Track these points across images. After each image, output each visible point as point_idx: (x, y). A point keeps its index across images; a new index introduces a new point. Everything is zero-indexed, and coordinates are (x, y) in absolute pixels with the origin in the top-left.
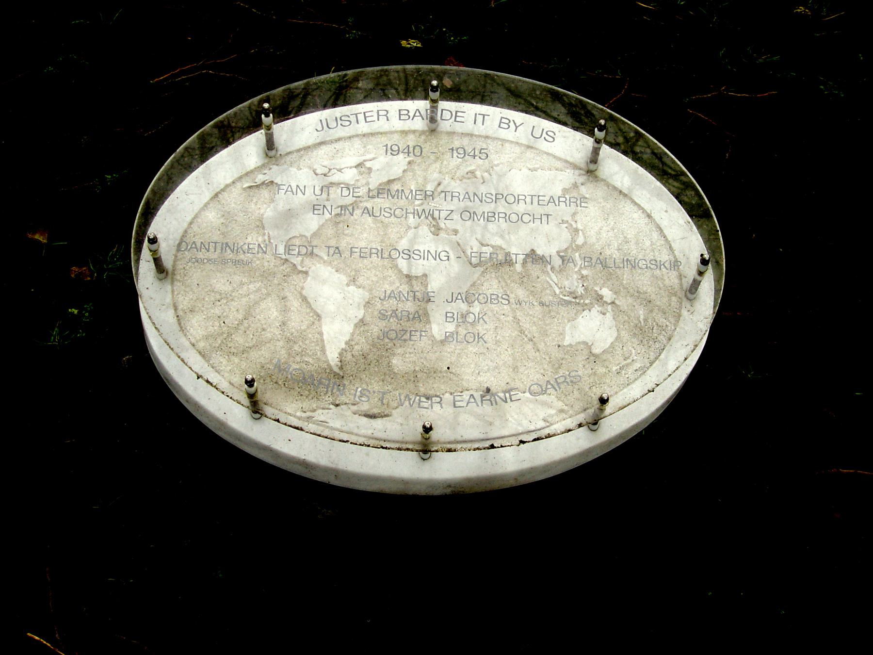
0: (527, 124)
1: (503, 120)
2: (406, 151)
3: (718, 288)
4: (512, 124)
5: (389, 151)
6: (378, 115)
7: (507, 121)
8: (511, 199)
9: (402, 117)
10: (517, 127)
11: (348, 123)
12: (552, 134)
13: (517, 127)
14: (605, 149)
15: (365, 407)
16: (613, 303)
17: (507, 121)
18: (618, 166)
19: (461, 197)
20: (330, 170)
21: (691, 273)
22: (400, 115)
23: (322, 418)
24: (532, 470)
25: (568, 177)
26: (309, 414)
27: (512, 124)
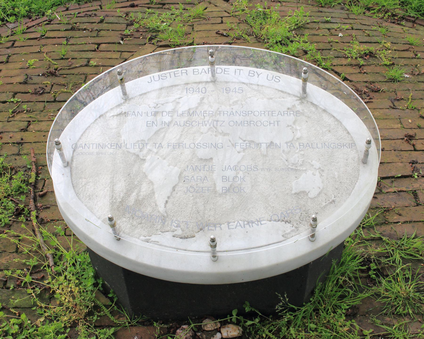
0: (264, 76)
1: (251, 72)
2: (198, 90)
3: (372, 127)
4: (256, 74)
5: (227, 179)
6: (182, 73)
7: (253, 72)
8: (256, 113)
9: (195, 73)
10: (258, 75)
11: (165, 78)
12: (278, 78)
13: (258, 75)
14: (309, 85)
15: (179, 232)
16: (320, 168)
17: (253, 72)
18: (317, 93)
19: (229, 114)
20: (157, 105)
21: (362, 145)
22: (194, 72)
23: (157, 240)
24: (277, 266)
25: (290, 101)
26: (148, 238)
27: (256, 74)
